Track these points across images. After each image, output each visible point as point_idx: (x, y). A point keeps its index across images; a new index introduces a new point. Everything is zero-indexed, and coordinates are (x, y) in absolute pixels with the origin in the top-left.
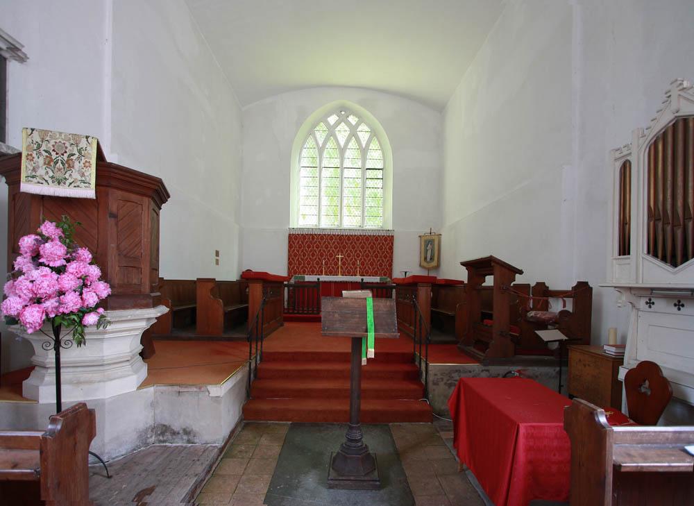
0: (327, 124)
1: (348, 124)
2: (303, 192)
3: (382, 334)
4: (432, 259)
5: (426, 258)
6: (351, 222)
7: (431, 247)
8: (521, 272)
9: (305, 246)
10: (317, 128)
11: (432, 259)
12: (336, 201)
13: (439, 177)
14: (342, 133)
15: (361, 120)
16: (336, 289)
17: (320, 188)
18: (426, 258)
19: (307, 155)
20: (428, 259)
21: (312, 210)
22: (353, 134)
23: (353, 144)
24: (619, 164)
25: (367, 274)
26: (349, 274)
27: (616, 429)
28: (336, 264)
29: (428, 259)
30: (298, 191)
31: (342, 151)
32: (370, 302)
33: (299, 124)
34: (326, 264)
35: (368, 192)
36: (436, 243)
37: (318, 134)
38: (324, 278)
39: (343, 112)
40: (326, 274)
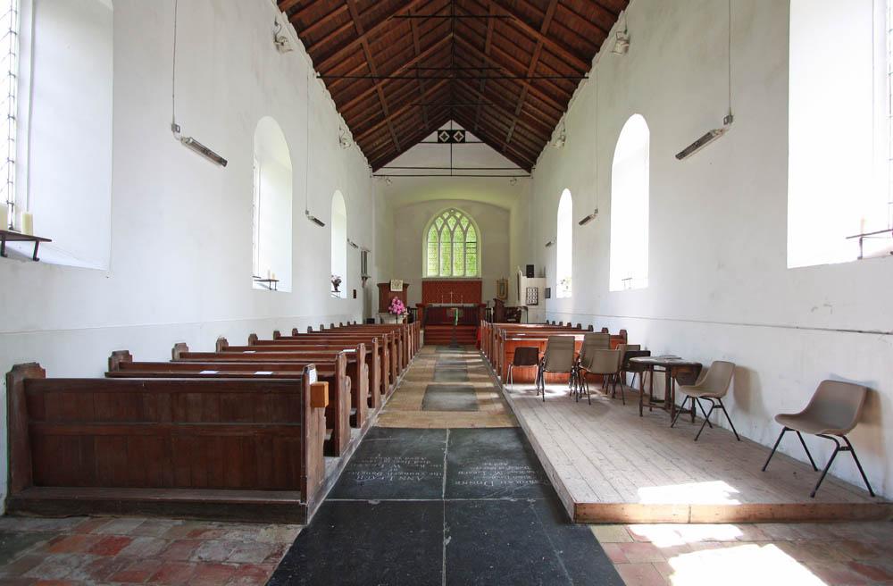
1: (455, 217)
13: (507, 247)
14: (452, 222)
15: (463, 215)
16: (450, 308)
19: (432, 232)
21: (432, 268)
22: (458, 222)
23: (458, 229)
24: (583, 226)
25: (467, 302)
38: (443, 305)
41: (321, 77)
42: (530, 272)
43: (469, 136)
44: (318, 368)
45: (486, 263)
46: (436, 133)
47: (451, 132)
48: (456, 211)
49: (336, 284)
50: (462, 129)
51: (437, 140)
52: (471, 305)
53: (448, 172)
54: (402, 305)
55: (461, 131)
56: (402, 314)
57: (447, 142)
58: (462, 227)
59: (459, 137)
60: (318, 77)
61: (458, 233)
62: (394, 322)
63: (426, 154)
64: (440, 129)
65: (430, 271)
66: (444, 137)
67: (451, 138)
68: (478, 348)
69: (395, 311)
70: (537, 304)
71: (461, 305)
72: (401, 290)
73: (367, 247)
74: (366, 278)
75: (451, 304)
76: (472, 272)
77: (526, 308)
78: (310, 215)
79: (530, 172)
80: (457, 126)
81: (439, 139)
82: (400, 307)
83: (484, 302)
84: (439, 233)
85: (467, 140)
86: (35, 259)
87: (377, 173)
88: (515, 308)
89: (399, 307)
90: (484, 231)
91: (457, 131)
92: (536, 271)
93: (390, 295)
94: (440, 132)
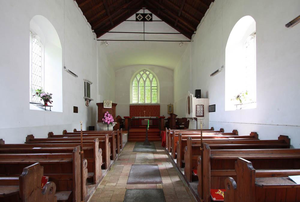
0: (140, 74)
2: (133, 93)
3: (150, 124)
4: (171, 111)
5: (169, 111)
6: (148, 102)
7: (171, 108)
8: (177, 116)
9: (135, 108)
10: (137, 75)
11: (171, 111)
12: (143, 96)
13: (172, 89)
14: (145, 76)
15: (150, 73)
16: (144, 119)
17: (138, 90)
18: (169, 111)
19: (135, 83)
20: (170, 111)
22: (148, 76)
23: (148, 80)
25: (153, 116)
26: (147, 116)
27: (257, 171)
28: (144, 113)
29: (170, 111)
30: (132, 93)
31: (145, 82)
32: (148, 120)
33: (132, 75)
34: (141, 113)
35: (153, 90)
36: (172, 107)
37: (137, 77)
38: (140, 117)
39: (145, 71)
40: (141, 116)
41: (95, 32)
42: (198, 94)
43: (155, 17)
44: (99, 139)
45: (162, 97)
46: (135, 15)
47: (144, 15)
48: (147, 71)
49: (47, 99)
50: (150, 13)
51: (135, 20)
52: (155, 117)
53: (140, 37)
54: (112, 117)
55: (150, 14)
56: (111, 123)
57: (141, 21)
58: (149, 79)
59: (148, 17)
60: (93, 32)
61: (148, 83)
62: (105, 129)
63: (130, 27)
64: (138, 13)
65: (134, 100)
66: (140, 17)
67: (144, 19)
68: (164, 146)
69: (106, 121)
70: (203, 116)
71: (150, 117)
72: (111, 107)
73: (91, 80)
74: (90, 100)
75: (145, 117)
76: (155, 101)
77: (196, 119)
78: (67, 69)
79: (190, 38)
80: (147, 11)
81: (136, 18)
82: (109, 119)
83: (161, 115)
84: (138, 82)
85: (153, 20)
86: (50, 110)
87: (100, 38)
88: (186, 119)
89: (109, 118)
90: (161, 80)
91: (148, 14)
92: (203, 93)
93: (104, 111)
94: (137, 15)
